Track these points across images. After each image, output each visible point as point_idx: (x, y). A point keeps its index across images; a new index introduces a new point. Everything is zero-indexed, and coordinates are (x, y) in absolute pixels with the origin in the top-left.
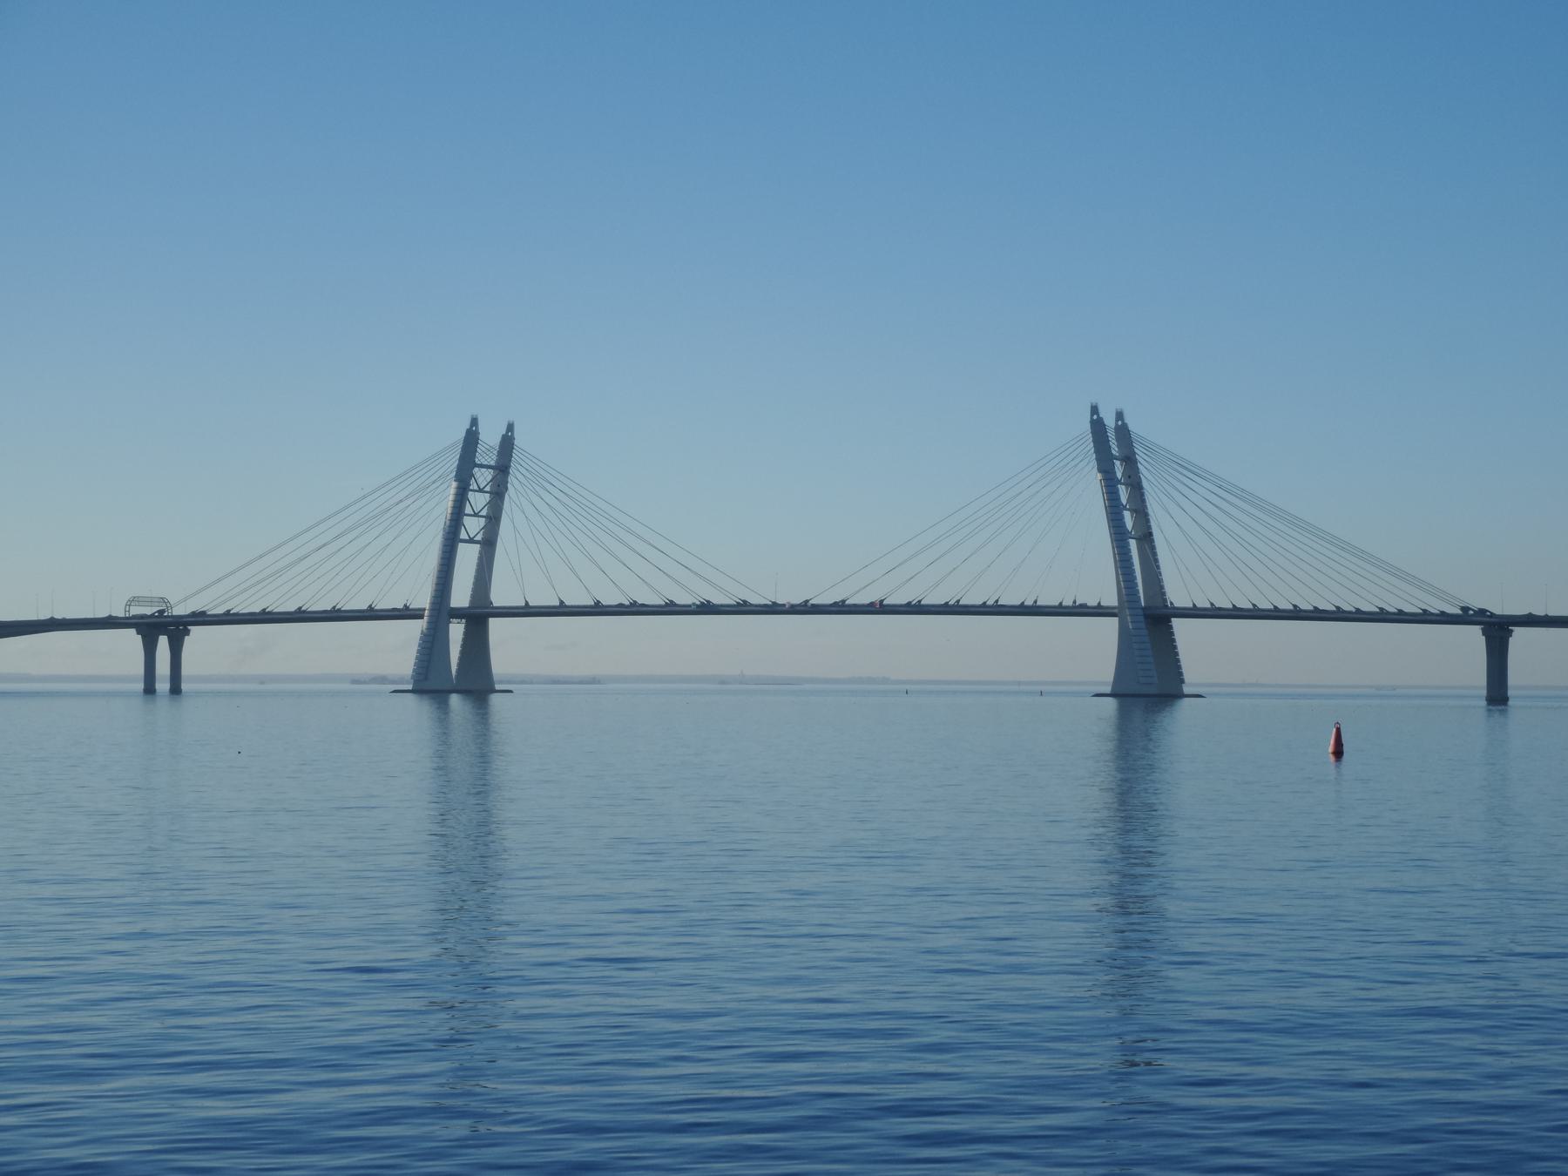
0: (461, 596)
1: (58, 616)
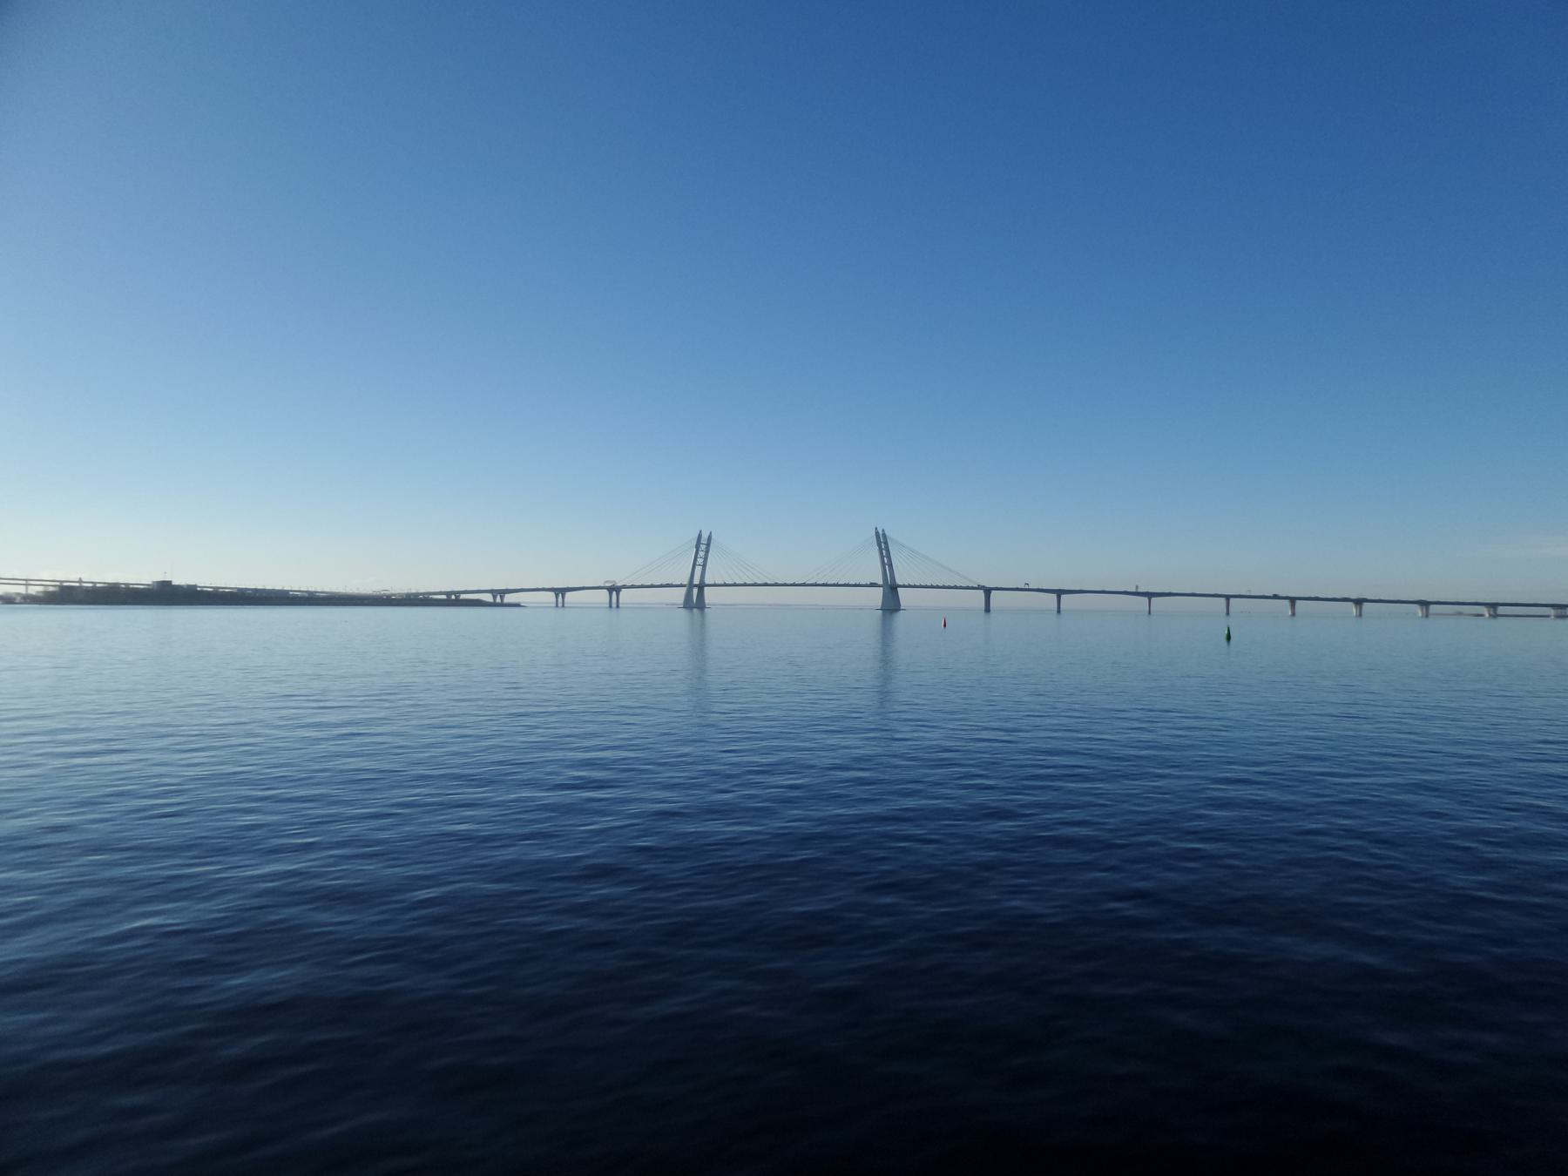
0: (696, 581)
1: (178, 580)
